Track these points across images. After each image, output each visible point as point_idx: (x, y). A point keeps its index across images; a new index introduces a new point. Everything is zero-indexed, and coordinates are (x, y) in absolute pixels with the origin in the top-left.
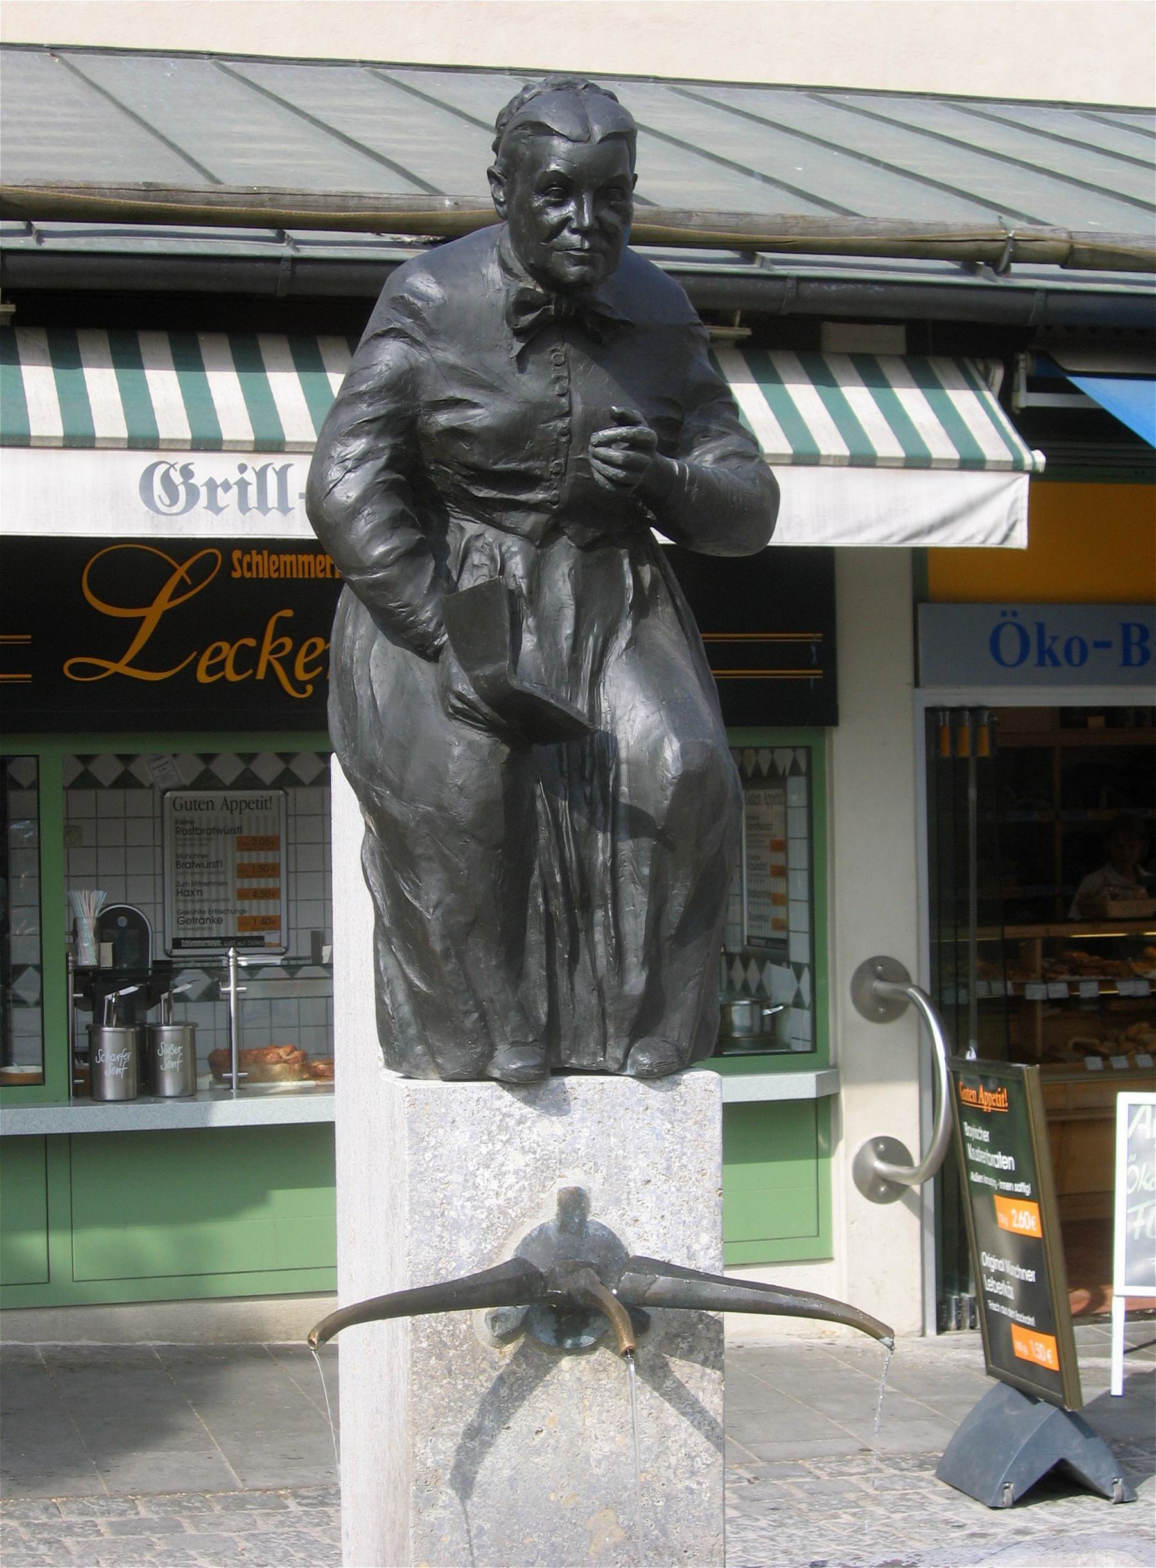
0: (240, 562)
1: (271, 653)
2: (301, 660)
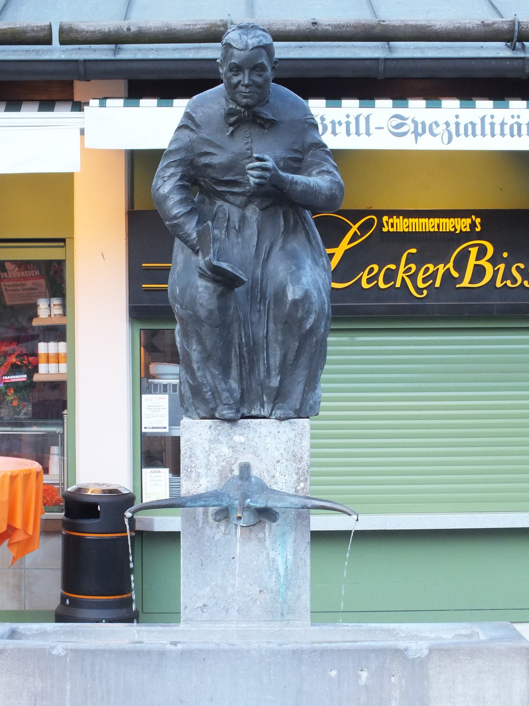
0: (387, 222)
1: (404, 273)
2: (420, 276)
